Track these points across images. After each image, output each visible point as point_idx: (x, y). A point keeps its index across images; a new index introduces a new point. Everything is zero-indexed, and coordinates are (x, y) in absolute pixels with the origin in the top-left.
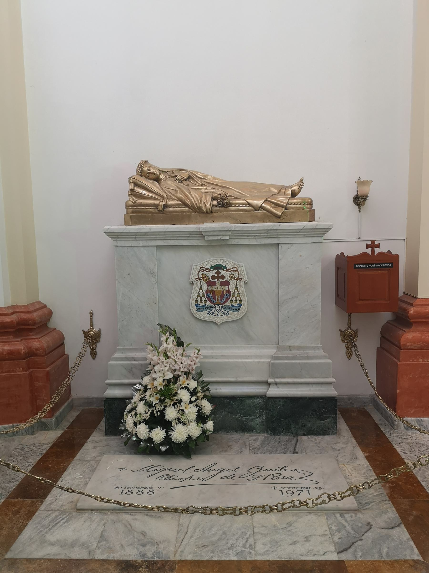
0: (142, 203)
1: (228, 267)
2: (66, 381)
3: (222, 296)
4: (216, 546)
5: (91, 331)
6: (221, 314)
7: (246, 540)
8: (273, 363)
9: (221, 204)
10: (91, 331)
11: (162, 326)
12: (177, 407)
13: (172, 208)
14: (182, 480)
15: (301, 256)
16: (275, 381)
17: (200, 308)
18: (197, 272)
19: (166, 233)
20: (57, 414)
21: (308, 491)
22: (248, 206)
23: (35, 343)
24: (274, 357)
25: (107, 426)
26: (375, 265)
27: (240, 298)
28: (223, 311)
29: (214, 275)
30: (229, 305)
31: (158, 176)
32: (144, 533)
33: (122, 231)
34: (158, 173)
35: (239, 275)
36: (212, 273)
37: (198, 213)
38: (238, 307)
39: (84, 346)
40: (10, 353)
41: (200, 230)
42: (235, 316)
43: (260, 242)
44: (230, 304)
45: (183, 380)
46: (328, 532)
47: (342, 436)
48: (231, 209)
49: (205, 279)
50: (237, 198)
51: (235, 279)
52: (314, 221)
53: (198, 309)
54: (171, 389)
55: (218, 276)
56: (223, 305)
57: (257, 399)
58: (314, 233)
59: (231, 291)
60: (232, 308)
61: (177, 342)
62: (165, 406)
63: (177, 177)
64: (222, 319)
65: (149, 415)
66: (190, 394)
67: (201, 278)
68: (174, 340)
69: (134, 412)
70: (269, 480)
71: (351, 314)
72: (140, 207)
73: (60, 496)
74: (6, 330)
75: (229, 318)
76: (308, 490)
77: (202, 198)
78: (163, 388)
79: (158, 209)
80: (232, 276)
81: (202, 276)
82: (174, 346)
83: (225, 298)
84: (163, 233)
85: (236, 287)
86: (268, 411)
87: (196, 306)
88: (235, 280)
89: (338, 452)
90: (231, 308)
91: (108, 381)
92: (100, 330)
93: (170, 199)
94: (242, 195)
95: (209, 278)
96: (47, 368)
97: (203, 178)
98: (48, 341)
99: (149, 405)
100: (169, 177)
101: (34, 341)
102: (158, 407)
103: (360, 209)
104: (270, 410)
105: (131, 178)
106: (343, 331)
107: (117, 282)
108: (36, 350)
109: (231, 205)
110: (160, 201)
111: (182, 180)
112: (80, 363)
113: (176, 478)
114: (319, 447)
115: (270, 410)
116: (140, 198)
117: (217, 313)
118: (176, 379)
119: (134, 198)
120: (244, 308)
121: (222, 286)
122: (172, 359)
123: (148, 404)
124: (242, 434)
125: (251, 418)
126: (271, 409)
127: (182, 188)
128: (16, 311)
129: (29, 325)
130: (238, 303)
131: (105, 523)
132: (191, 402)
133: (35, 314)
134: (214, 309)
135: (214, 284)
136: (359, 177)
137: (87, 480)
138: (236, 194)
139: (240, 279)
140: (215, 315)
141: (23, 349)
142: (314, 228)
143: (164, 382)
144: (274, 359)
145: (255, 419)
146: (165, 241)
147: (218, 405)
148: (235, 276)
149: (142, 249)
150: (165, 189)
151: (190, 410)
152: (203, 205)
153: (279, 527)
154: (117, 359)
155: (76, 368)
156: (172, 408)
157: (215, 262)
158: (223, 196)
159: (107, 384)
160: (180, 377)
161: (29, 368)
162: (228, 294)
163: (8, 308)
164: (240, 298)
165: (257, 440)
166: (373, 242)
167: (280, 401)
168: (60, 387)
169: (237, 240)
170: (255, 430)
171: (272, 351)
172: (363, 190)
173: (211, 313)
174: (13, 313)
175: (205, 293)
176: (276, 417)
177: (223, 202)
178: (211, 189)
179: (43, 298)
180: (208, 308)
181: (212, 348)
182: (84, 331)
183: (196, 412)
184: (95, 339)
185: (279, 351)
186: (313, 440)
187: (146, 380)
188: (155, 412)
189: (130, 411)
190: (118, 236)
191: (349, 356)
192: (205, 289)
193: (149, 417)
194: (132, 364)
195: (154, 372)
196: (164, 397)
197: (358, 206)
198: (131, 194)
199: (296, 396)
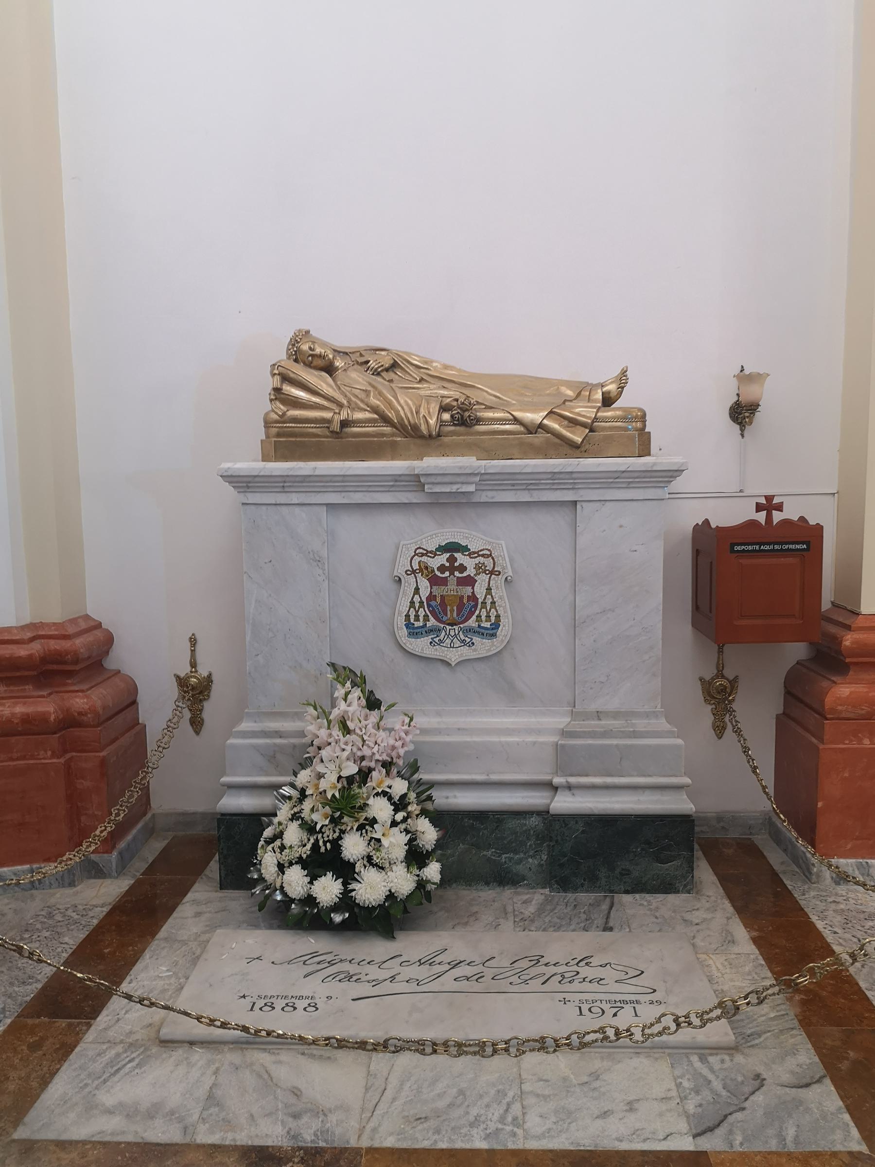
0: (299, 417)
2: (140, 778)
4: (444, 1120)
5: (192, 677)
6: (457, 643)
7: (505, 1108)
8: (563, 746)
9: (458, 420)
11: (336, 667)
13: (359, 427)
14: (376, 983)
15: (621, 526)
16: (567, 781)
17: (414, 632)
18: (409, 559)
20: (122, 845)
21: (634, 1008)
23: (78, 700)
25: (222, 871)
26: (774, 547)
27: (497, 611)
28: (462, 637)
29: (443, 565)
30: (474, 625)
32: (295, 1091)
36: (439, 560)
37: (412, 437)
38: (493, 629)
39: (178, 706)
40: (26, 719)
41: (416, 473)
42: (487, 648)
44: (477, 623)
45: (379, 779)
46: (674, 1093)
47: (703, 895)
48: (481, 430)
49: (425, 571)
51: (487, 572)
52: (649, 454)
53: (409, 634)
54: (355, 797)
55: (452, 567)
56: (461, 626)
57: (530, 818)
59: (478, 597)
60: (480, 632)
61: (368, 700)
62: (343, 832)
64: (459, 653)
65: (309, 849)
66: (393, 807)
67: (416, 569)
68: (361, 695)
69: (278, 843)
70: (553, 984)
72: (293, 425)
73: (125, 1014)
74: (18, 674)
75: (475, 653)
76: (634, 1005)
77: (420, 406)
78: (337, 795)
80: (480, 565)
81: (420, 566)
82: (360, 709)
83: (465, 612)
85: (489, 589)
86: (552, 844)
87: (407, 626)
89: (695, 928)
90: (479, 633)
91: (224, 779)
92: (210, 674)
95: (433, 571)
96: (102, 750)
97: (422, 365)
99: (310, 828)
101: (76, 697)
102: (327, 833)
103: (742, 430)
104: (557, 841)
105: (276, 367)
107: (245, 576)
108: (80, 714)
109: (478, 421)
110: (335, 413)
111: (379, 370)
112: (178, 722)
113: (364, 978)
114: (656, 918)
115: (557, 841)
116: (293, 407)
117: (448, 641)
118: (364, 775)
119: (282, 407)
120: (504, 631)
121: (460, 587)
122: (358, 735)
124: (498, 890)
125: (517, 856)
126: (559, 838)
127: (380, 387)
129: (65, 663)
131: (218, 1069)
132: (394, 824)
134: (443, 634)
135: (444, 582)
137: (181, 980)
138: (490, 400)
139: (497, 573)
140: (444, 645)
142: (650, 469)
143: (340, 782)
144: (566, 737)
146: (343, 494)
148: (486, 566)
149: (297, 510)
150: (346, 387)
151: (392, 839)
152: (422, 421)
153: (574, 1080)
154: (245, 734)
157: (447, 537)
158: (463, 403)
159: (223, 785)
161: (65, 751)
162: (473, 603)
163: (23, 628)
164: (497, 611)
165: (531, 902)
166: (769, 498)
167: (577, 823)
168: (128, 791)
169: (490, 494)
170: (525, 882)
171: (562, 721)
172: (750, 393)
173: (437, 641)
174: (32, 639)
175: (424, 600)
177: (462, 416)
178: (439, 388)
179: (95, 612)
180: (431, 631)
181: (439, 714)
182: (177, 677)
183: (406, 845)
184: (201, 692)
185: (575, 721)
186: (645, 903)
187: (304, 777)
188: (321, 843)
189: (270, 841)
190: (249, 482)
191: (719, 731)
192: (425, 592)
193: (308, 853)
194: (275, 744)
195: (319, 761)
196: (339, 813)
197: (740, 425)
198: (276, 399)
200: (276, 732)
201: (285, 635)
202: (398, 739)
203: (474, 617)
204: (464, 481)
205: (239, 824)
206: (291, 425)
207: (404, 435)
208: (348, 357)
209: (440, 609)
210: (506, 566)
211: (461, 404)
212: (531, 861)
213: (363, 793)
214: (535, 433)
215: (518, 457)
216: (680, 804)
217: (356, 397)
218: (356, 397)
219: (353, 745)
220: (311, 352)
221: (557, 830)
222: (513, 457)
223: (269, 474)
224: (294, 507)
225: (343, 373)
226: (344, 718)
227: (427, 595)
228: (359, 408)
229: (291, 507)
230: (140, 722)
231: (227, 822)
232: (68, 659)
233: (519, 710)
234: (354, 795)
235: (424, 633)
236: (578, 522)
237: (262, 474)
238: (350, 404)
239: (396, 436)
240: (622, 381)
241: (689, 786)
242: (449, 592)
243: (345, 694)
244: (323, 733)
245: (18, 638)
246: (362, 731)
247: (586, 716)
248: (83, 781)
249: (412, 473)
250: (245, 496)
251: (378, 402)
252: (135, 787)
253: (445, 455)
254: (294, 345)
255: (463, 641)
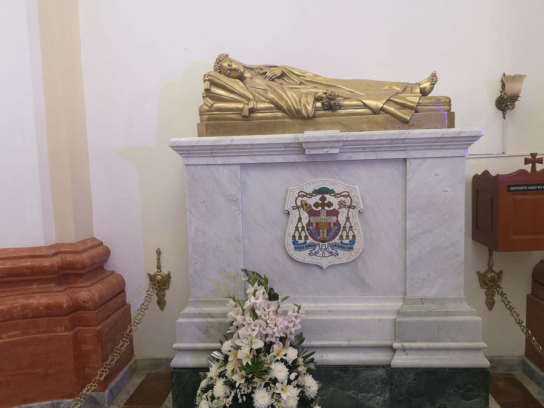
0: (222, 107)
1: (337, 191)
2: (120, 345)
3: (329, 230)
5: (158, 275)
6: (327, 254)
8: (400, 322)
9: (327, 106)
10: (158, 275)
11: (248, 272)
12: (271, 389)
13: (261, 113)
15: (437, 175)
16: (403, 346)
17: (298, 247)
18: (295, 199)
19: (253, 147)
20: (112, 384)
22: (363, 108)
23: (82, 293)
24: (399, 313)
26: (537, 187)
28: (331, 250)
29: (317, 202)
30: (338, 242)
31: (242, 74)
33: (194, 145)
34: (242, 70)
35: (351, 201)
37: (296, 118)
38: (351, 244)
39: (149, 294)
40: (48, 307)
41: (300, 141)
42: (347, 257)
43: (381, 157)
44: (340, 241)
45: (278, 350)
48: (342, 113)
50: (348, 98)
51: (347, 207)
52: (454, 127)
53: (295, 248)
54: (261, 363)
55: (323, 204)
56: (330, 242)
57: (377, 370)
58: (456, 143)
59: (341, 223)
60: (342, 246)
61: (269, 294)
62: (254, 388)
63: (267, 74)
64: (329, 260)
66: (288, 370)
67: (300, 206)
68: (265, 291)
69: (209, 393)
71: (492, 252)
72: (218, 113)
74: (45, 277)
75: (339, 260)
77: (301, 98)
78: (250, 363)
79: (243, 115)
80: (342, 202)
81: (302, 203)
82: (264, 301)
84: (249, 147)
85: (348, 218)
86: (393, 387)
87: (294, 243)
88: (346, 208)
90: (341, 247)
91: (175, 345)
92: (169, 273)
93: (257, 101)
94: (355, 94)
95: (310, 207)
96: (98, 325)
97: (301, 74)
98: (101, 290)
99: (231, 385)
100: (256, 74)
101: (82, 291)
102: (243, 389)
103: (504, 114)
104: (396, 386)
105: (207, 75)
106: (482, 273)
107: (188, 212)
108: (84, 302)
109: (340, 107)
110: (245, 104)
111: (273, 77)
112: (148, 305)
115: (396, 386)
116: (218, 101)
118: (268, 346)
119: (211, 101)
121: (328, 217)
122: (263, 319)
123: (230, 383)
125: (369, 395)
126: (398, 384)
127: (275, 87)
128: (60, 251)
129: (76, 269)
130: (351, 239)
132: (289, 382)
133: (85, 255)
134: (318, 248)
135: (318, 214)
136: (503, 74)
138: (347, 94)
139: (353, 207)
140: (318, 255)
141: (65, 301)
142: (458, 136)
143: (252, 353)
144: (401, 316)
145: (375, 397)
146: (251, 157)
147: (325, 378)
148: (346, 203)
149: (221, 168)
150: (252, 88)
151: (288, 394)
152: (303, 108)
154: (188, 316)
155: (136, 326)
156: (264, 391)
157: (319, 184)
158: (330, 95)
159: (175, 349)
160: (274, 345)
161: (74, 326)
162: (337, 228)
163: (50, 247)
166: (533, 155)
167: (410, 373)
168: (111, 356)
169: (349, 155)
171: (397, 305)
172: (510, 89)
173: (314, 253)
174: (56, 254)
175: (305, 226)
176: (404, 395)
177: (329, 103)
178: (312, 88)
179: (99, 234)
180: (309, 246)
181: (315, 301)
182: (149, 275)
183: (298, 396)
184: (164, 284)
187: (227, 346)
188: (239, 396)
189: (205, 391)
190: (189, 151)
191: (490, 306)
192: (305, 221)
193: (230, 403)
194: (208, 322)
195: (237, 336)
196: (251, 375)
197: (502, 111)
198: (207, 96)
199: (432, 366)
200: (209, 314)
201: (214, 250)
202: (290, 321)
203: (338, 237)
204: (332, 146)
205: (185, 375)
206: (216, 113)
207: (291, 117)
208: (253, 71)
209: (315, 231)
210: (359, 202)
211: (329, 96)
212: (378, 398)
213: (267, 360)
214: (379, 114)
215: (367, 130)
216: (481, 361)
217: (259, 93)
218: (259, 93)
219: (260, 327)
220: (229, 67)
221: (396, 379)
222: (363, 130)
223: (203, 145)
224: (219, 166)
225: (250, 80)
226: (253, 307)
227: (307, 222)
228: (260, 101)
229: (217, 167)
230: (127, 303)
231: (177, 373)
232: (78, 266)
233: (369, 297)
234: (262, 362)
235: (305, 247)
236: (408, 172)
237: (197, 145)
238: (254, 98)
239: (286, 118)
240: (434, 80)
241: (485, 348)
242: (321, 220)
243: (254, 291)
244: (239, 318)
245: (45, 254)
246: (266, 317)
247: (414, 301)
248: (86, 346)
249: (297, 142)
250: (187, 159)
251: (273, 96)
252: (116, 353)
253: (318, 129)
254: (218, 63)
255: (331, 253)
